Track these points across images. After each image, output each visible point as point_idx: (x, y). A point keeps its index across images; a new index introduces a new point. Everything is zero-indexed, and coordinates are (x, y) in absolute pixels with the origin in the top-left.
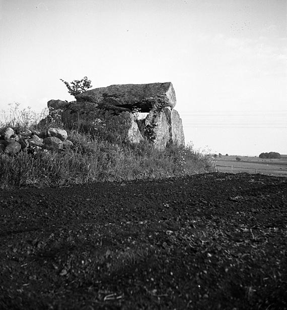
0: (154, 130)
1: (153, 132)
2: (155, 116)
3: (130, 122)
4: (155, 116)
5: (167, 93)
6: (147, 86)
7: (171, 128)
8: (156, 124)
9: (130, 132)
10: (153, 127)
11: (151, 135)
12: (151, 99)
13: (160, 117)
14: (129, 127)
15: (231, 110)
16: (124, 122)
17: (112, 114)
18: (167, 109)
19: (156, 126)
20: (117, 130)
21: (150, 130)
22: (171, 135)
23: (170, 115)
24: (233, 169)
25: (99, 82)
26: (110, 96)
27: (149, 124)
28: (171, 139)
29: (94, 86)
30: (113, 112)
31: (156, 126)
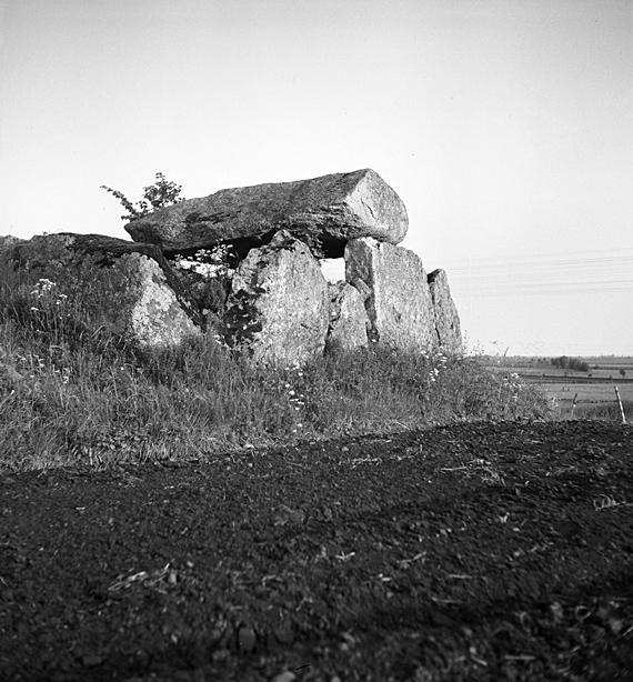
0: (259, 304)
1: (255, 310)
2: (262, 264)
3: (139, 284)
4: (262, 264)
5: (348, 199)
6: (303, 187)
7: (373, 295)
8: (263, 287)
9: (140, 315)
10: (256, 297)
11: (248, 319)
12: (315, 218)
13: (277, 265)
14: (134, 301)
15: (537, 241)
16: (124, 285)
17: (97, 264)
18: (363, 245)
19: (263, 291)
20: (106, 309)
21: (244, 305)
22: (373, 317)
23: (371, 260)
24: (558, 401)
25: (196, 186)
26: (205, 219)
27: (246, 288)
28: (374, 327)
29: (188, 193)
30: (101, 257)
31: (263, 291)
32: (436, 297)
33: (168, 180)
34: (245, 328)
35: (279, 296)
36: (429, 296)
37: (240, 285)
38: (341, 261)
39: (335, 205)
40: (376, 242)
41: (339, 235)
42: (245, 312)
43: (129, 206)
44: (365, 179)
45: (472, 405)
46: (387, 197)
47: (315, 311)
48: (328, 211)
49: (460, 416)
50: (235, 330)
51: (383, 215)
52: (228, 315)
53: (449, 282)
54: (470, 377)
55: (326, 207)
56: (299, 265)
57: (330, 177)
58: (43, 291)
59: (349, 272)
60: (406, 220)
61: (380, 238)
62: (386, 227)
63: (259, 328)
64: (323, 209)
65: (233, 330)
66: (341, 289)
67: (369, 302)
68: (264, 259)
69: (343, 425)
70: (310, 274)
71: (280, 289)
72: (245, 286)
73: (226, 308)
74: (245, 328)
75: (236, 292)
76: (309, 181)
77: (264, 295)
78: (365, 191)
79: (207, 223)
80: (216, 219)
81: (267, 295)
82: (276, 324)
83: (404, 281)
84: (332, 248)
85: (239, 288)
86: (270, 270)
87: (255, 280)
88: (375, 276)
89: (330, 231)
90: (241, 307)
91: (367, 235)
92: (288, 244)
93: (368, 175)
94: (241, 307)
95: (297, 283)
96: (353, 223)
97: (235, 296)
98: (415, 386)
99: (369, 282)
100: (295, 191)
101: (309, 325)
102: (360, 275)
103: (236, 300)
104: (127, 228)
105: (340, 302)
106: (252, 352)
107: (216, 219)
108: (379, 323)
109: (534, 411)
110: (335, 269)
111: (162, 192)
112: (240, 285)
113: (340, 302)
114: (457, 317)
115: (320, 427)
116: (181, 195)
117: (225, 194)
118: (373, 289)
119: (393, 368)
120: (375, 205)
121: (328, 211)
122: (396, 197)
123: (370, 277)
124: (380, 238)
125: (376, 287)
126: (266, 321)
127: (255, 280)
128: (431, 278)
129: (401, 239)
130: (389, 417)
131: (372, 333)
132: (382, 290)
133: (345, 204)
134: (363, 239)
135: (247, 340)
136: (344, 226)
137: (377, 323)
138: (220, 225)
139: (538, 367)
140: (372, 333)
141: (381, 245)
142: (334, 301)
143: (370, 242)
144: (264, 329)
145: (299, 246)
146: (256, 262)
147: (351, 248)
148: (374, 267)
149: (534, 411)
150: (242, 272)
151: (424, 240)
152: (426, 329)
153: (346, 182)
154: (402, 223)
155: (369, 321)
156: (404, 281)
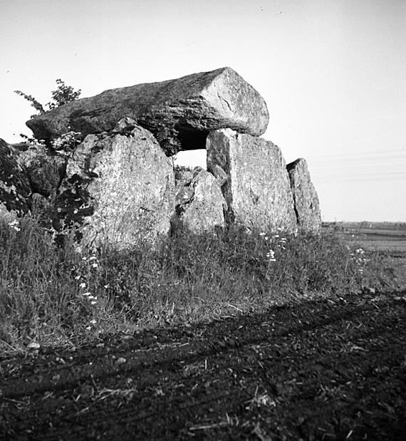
0: (91, 189)
1: (87, 194)
2: (96, 149)
4: (96, 149)
5: (204, 93)
6: (169, 85)
8: (94, 171)
10: (88, 182)
11: (80, 203)
13: (111, 150)
18: (222, 135)
19: (96, 176)
21: (77, 189)
22: (229, 200)
23: (228, 149)
27: (79, 172)
28: (230, 208)
31: (96, 176)
32: (296, 182)
33: (67, 85)
34: (76, 212)
35: (112, 180)
36: (287, 181)
37: (74, 169)
38: (204, 152)
39: (193, 98)
40: (235, 132)
41: (200, 126)
42: (77, 195)
43: (38, 106)
44: (222, 76)
45: (315, 282)
46: (245, 93)
47: (157, 193)
48: (186, 104)
49: (302, 293)
50: (65, 214)
51: (241, 109)
52: (61, 199)
53: (309, 169)
54: (315, 248)
55: (184, 100)
56: (137, 149)
57: (193, 76)
58: (42, 176)
59: (210, 159)
60: (266, 115)
61: (240, 129)
62: (245, 120)
63: (90, 212)
64: (181, 102)
65: (63, 214)
66: (195, 174)
67: (225, 187)
68: (100, 144)
69: (159, 316)
70: (152, 159)
71: (114, 173)
72: (79, 170)
73: (58, 192)
74: (76, 212)
75: (70, 177)
76: (176, 80)
77: (96, 179)
78: (221, 86)
79: (85, 117)
80: (94, 114)
81: (100, 180)
82: (108, 208)
83: (262, 168)
84: (192, 137)
85: (73, 173)
86: (104, 155)
87: (88, 166)
88: (232, 163)
89: (191, 122)
90: (73, 192)
91: (227, 127)
92: (128, 131)
93: (225, 72)
94: (73, 192)
95: (135, 168)
96: (211, 116)
97: (69, 180)
98: (256, 266)
99: (227, 168)
100: (162, 88)
101: (150, 208)
102: (219, 162)
103: (69, 184)
104: (29, 124)
105: (194, 186)
106: (79, 236)
107: (94, 114)
108: (235, 205)
109: (380, 280)
110: (194, 158)
111: (65, 95)
112: (74, 169)
113: (194, 186)
114: (316, 198)
115: (134, 316)
116: (80, 97)
117: (108, 95)
118: (230, 174)
119: (236, 246)
120: (233, 99)
121: (186, 104)
122: (257, 94)
123: (228, 163)
124: (240, 129)
125: (233, 172)
126: (97, 204)
127: (88, 166)
128: (291, 167)
129: (262, 132)
130: (220, 301)
131: (229, 214)
132: (239, 175)
133: (201, 97)
134: (223, 130)
135: (77, 224)
136: (203, 118)
137: (232, 205)
138: (96, 119)
139: (400, 229)
140: (229, 214)
141: (240, 136)
142: (188, 185)
143: (228, 133)
144: (95, 213)
145: (140, 132)
146: (90, 147)
147: (212, 137)
148: (231, 155)
149: (380, 280)
150: (75, 157)
151: (286, 133)
152: (285, 209)
153: (204, 79)
154: (262, 118)
155: (225, 203)
156: (262, 168)
